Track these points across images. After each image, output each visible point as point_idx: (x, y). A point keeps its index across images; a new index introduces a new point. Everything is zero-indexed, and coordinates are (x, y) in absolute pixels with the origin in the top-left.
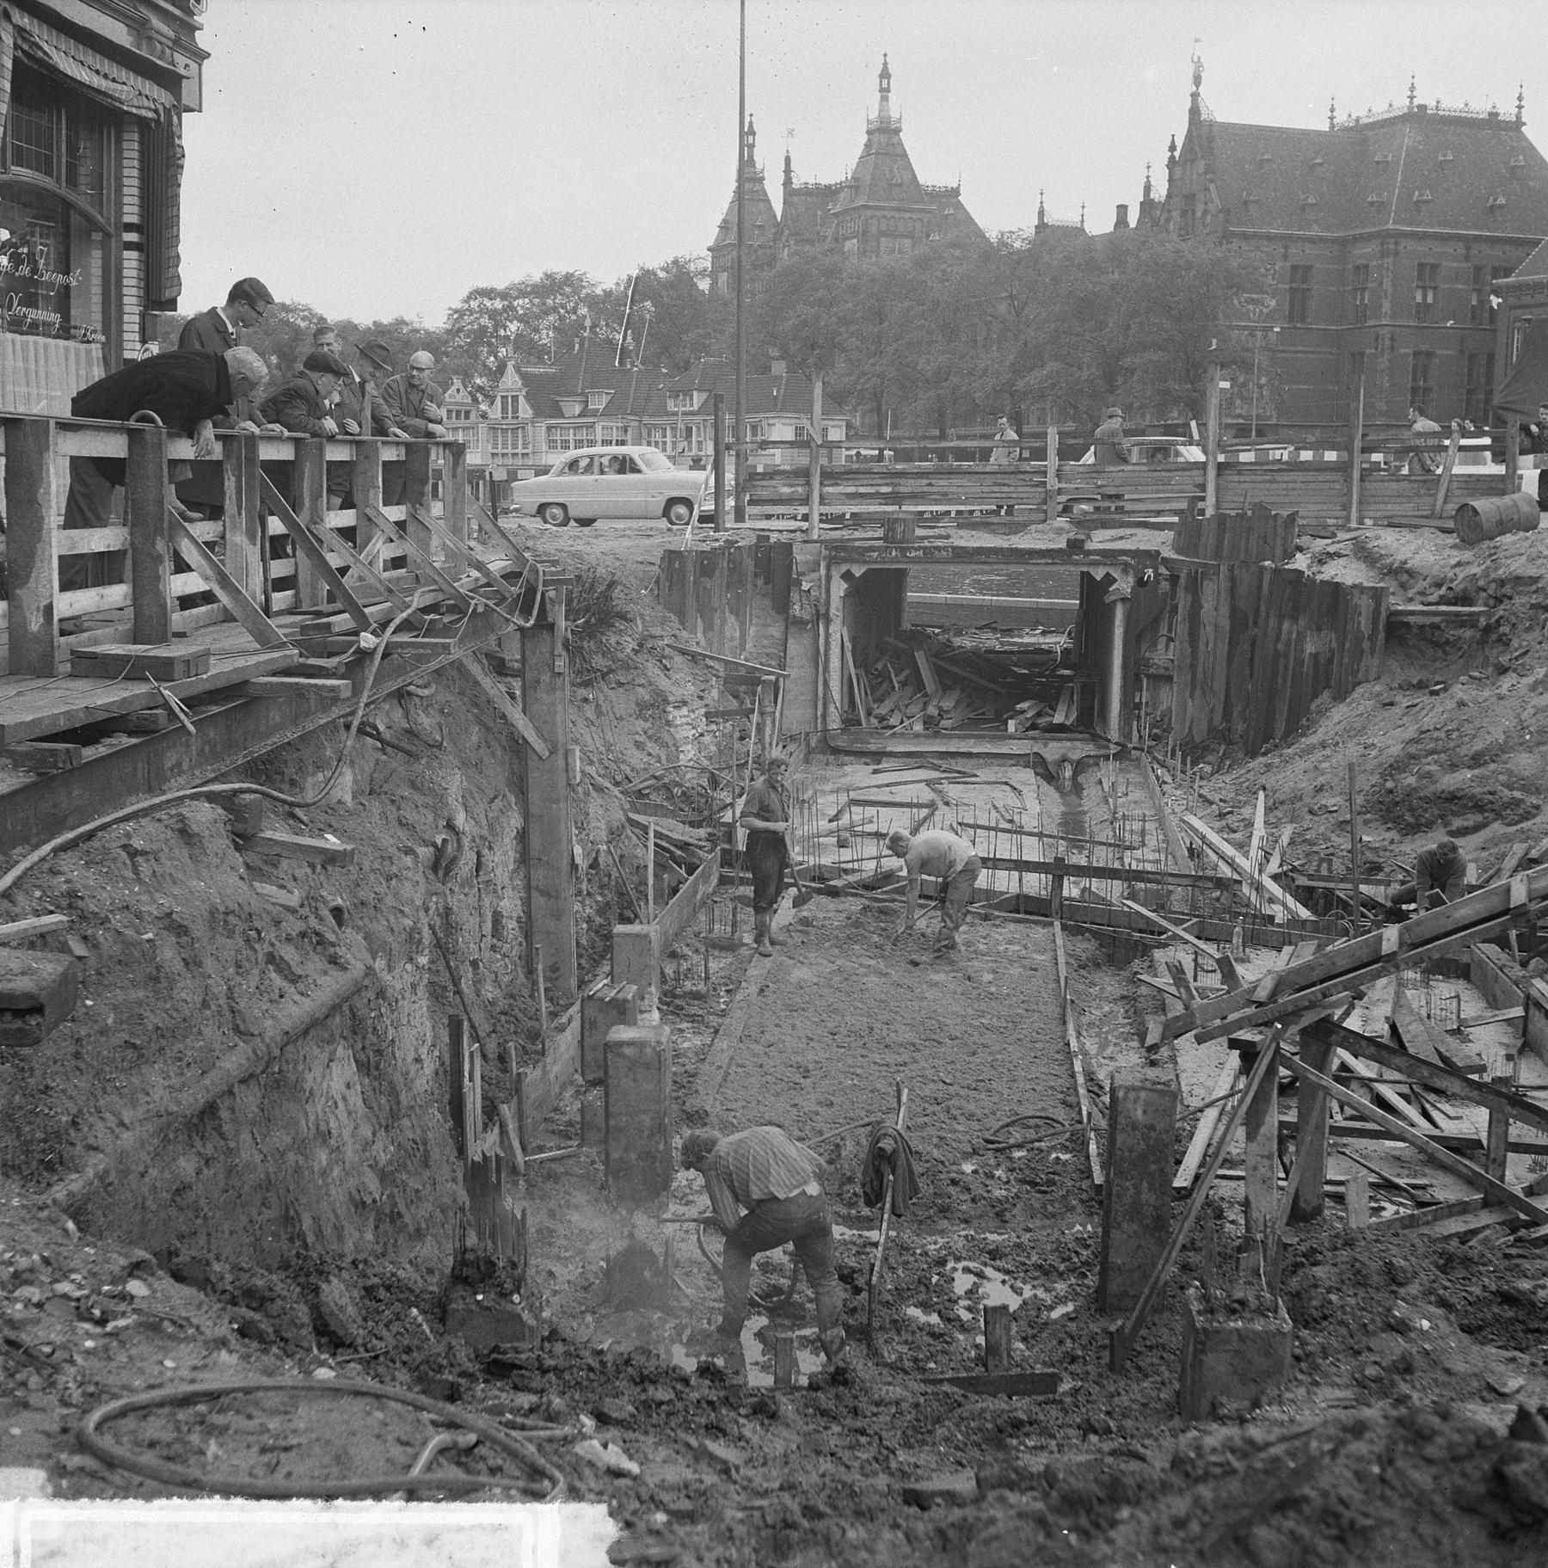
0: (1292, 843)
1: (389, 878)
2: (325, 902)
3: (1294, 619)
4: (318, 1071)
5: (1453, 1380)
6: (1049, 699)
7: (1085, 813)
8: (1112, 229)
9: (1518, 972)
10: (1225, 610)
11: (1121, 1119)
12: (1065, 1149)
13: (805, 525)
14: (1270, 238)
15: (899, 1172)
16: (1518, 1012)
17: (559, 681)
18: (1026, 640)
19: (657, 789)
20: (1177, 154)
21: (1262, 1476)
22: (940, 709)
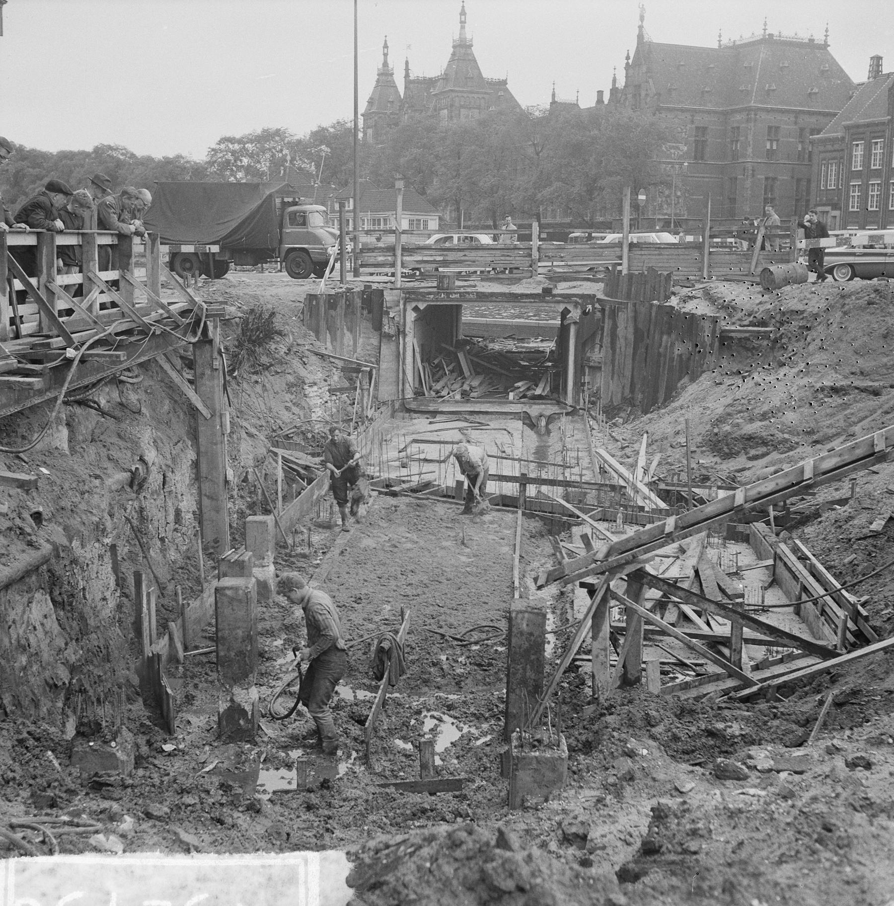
0: (660, 464)
1: (82, 493)
2: (29, 509)
3: (669, 334)
4: (19, 609)
5: (657, 784)
6: (535, 381)
7: (549, 446)
8: (594, 105)
9: (773, 538)
10: (631, 329)
11: (514, 629)
12: (502, 644)
13: (393, 279)
14: (682, 110)
15: (393, 660)
16: (770, 562)
17: (216, 374)
18: (531, 345)
19: (297, 434)
20: (630, 61)
21: (366, 868)
22: (471, 386)
